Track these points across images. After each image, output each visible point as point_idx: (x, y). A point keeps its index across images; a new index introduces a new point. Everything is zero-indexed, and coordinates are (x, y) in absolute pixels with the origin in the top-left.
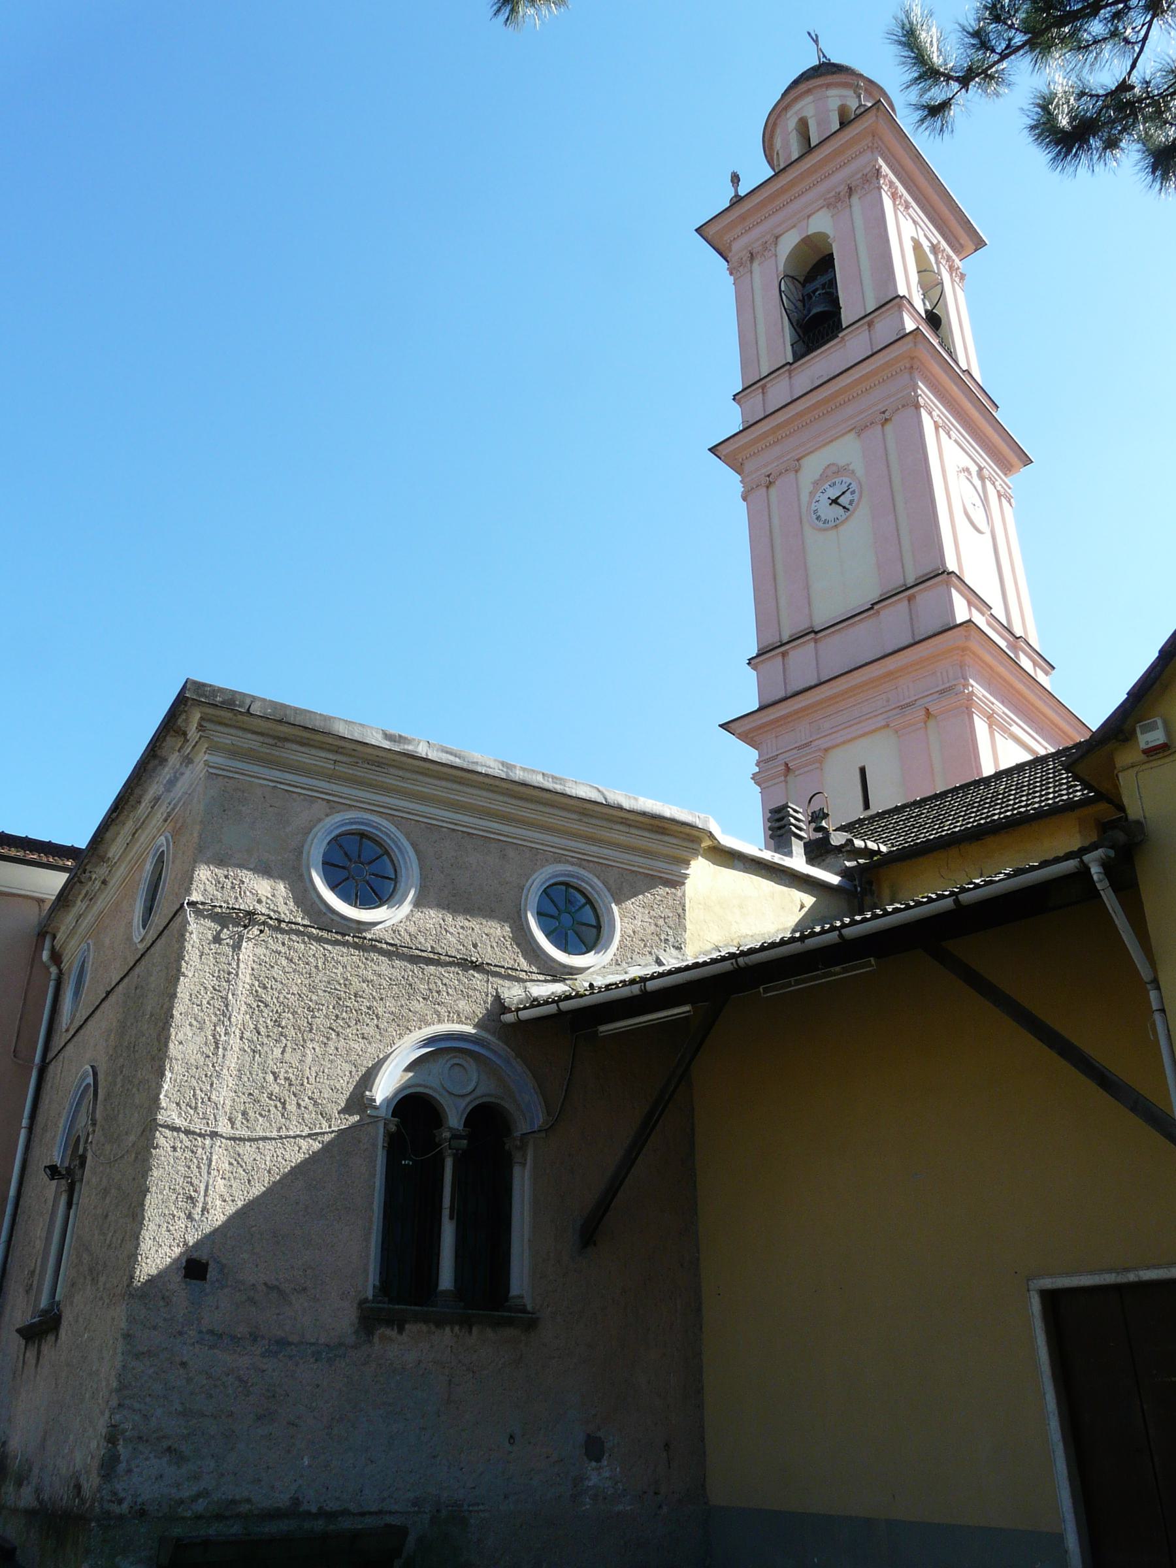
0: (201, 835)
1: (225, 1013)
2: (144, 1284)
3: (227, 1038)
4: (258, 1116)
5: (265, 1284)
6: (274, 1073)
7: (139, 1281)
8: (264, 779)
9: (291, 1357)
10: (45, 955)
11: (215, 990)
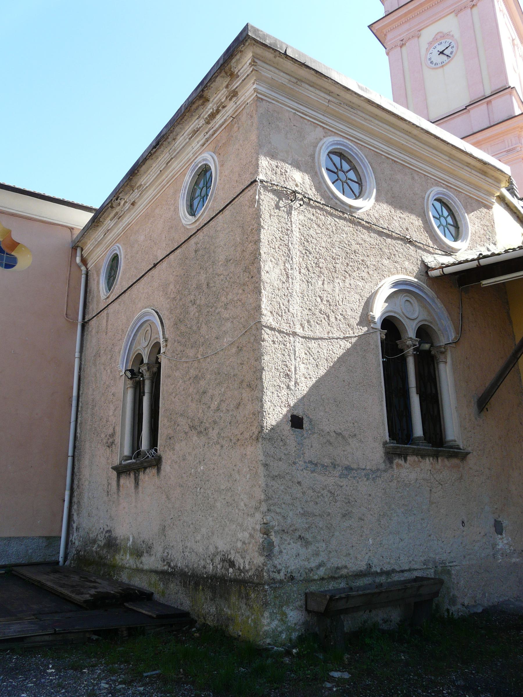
0: (259, 137)
1: (289, 256)
2: (270, 431)
3: (292, 272)
4: (316, 324)
5: (334, 431)
6: (320, 297)
7: (267, 429)
8: (289, 107)
9: (354, 477)
10: (78, 260)
11: (281, 240)
